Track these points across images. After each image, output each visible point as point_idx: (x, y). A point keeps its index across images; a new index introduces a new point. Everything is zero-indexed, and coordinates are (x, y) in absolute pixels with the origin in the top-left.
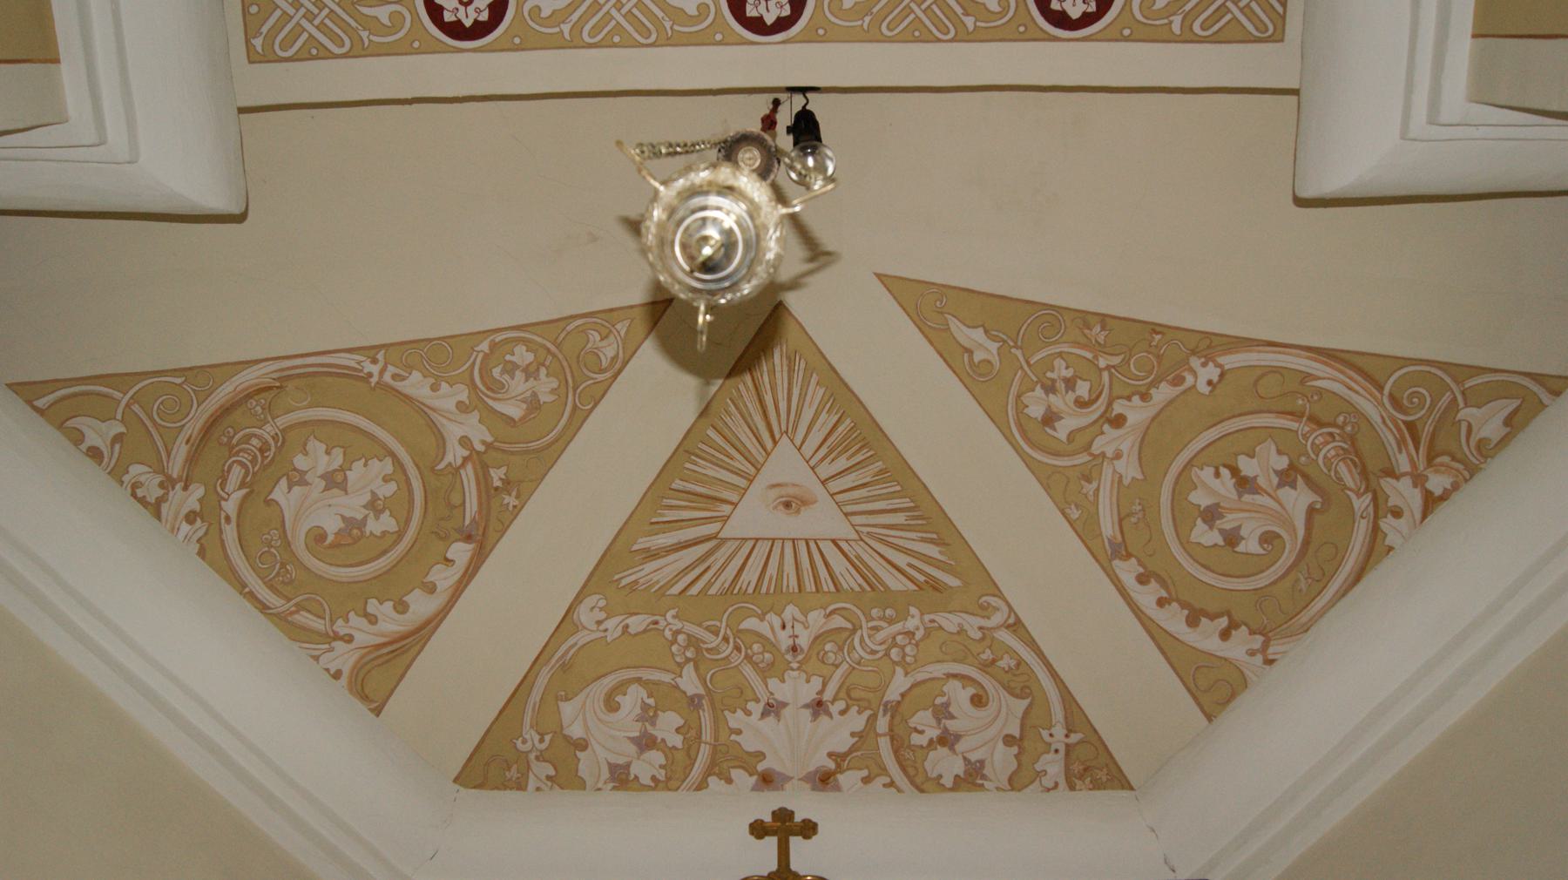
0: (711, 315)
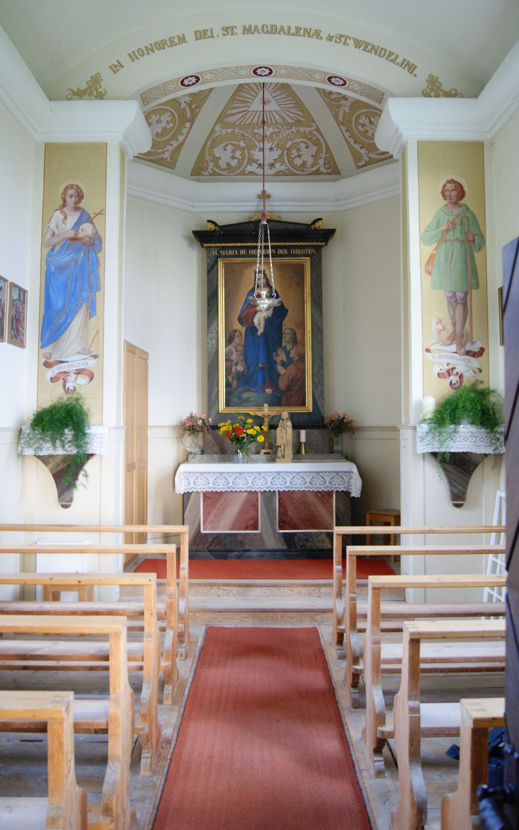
0: (268, 388)
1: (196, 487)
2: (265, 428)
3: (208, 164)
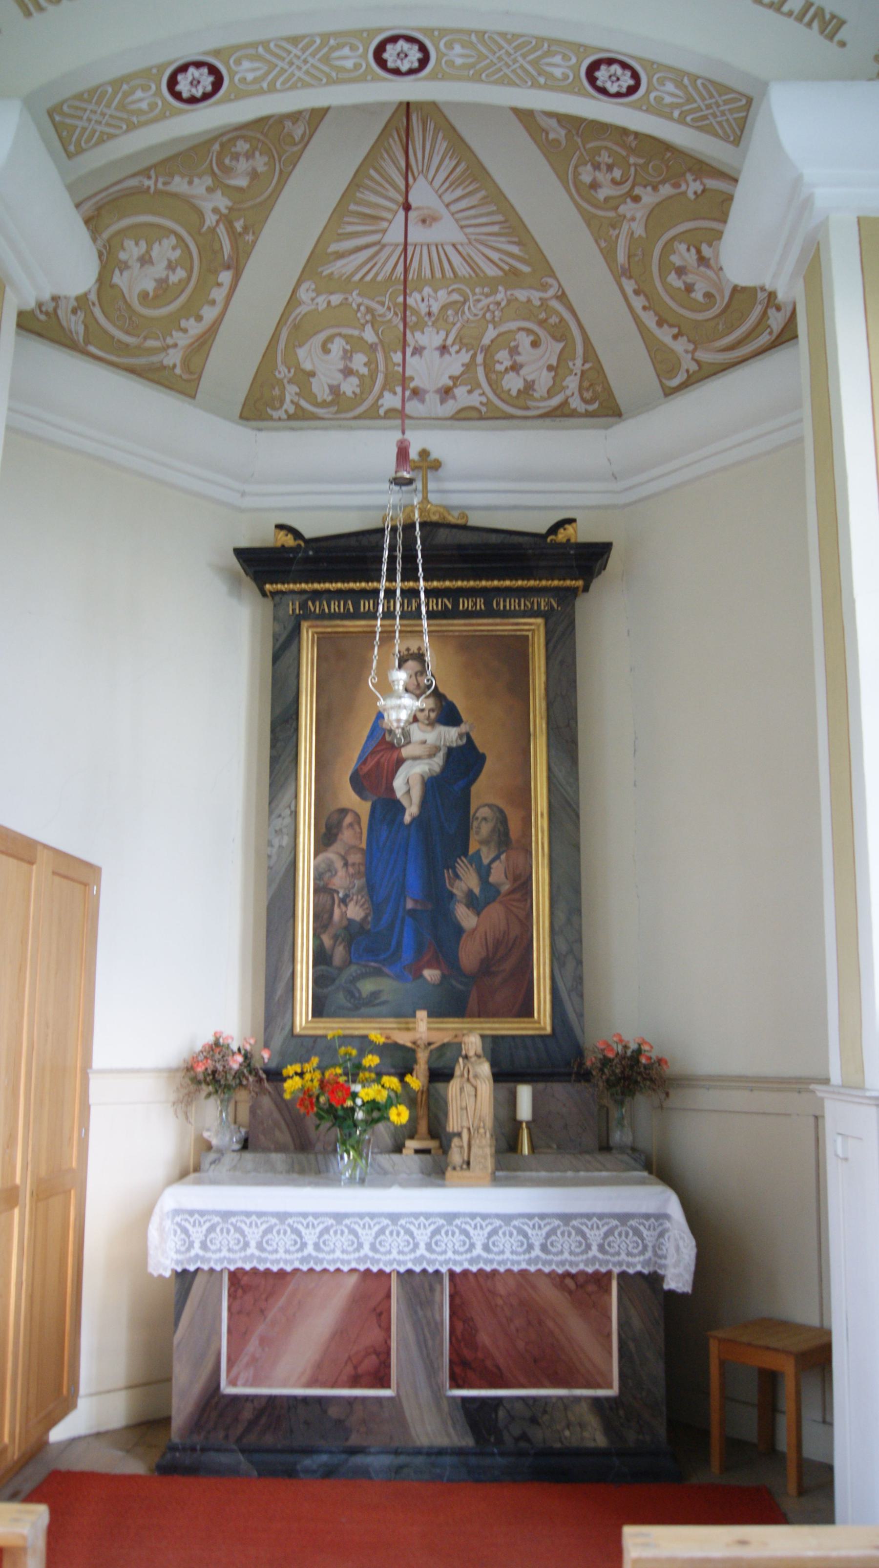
0: (430, 966)
1: (209, 1255)
2: (415, 1082)
3: (282, 391)
